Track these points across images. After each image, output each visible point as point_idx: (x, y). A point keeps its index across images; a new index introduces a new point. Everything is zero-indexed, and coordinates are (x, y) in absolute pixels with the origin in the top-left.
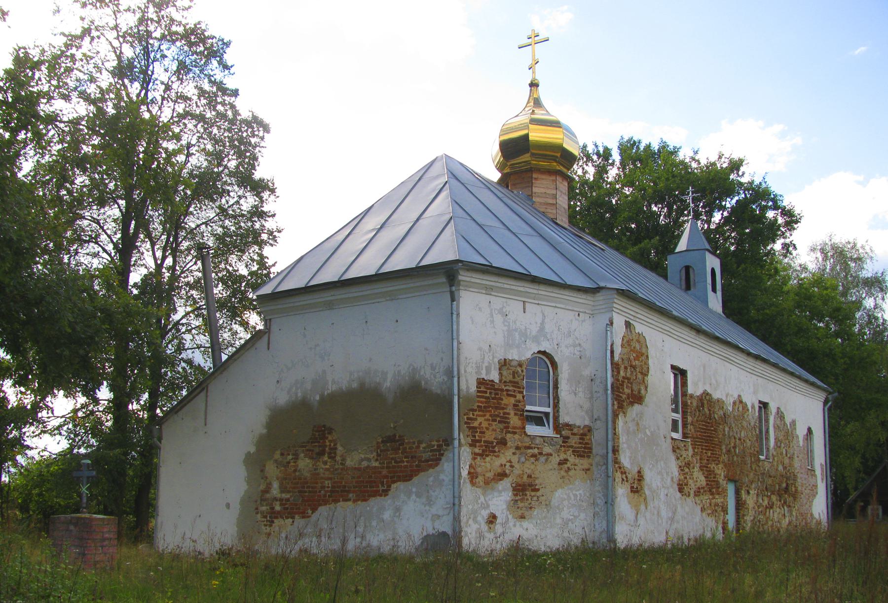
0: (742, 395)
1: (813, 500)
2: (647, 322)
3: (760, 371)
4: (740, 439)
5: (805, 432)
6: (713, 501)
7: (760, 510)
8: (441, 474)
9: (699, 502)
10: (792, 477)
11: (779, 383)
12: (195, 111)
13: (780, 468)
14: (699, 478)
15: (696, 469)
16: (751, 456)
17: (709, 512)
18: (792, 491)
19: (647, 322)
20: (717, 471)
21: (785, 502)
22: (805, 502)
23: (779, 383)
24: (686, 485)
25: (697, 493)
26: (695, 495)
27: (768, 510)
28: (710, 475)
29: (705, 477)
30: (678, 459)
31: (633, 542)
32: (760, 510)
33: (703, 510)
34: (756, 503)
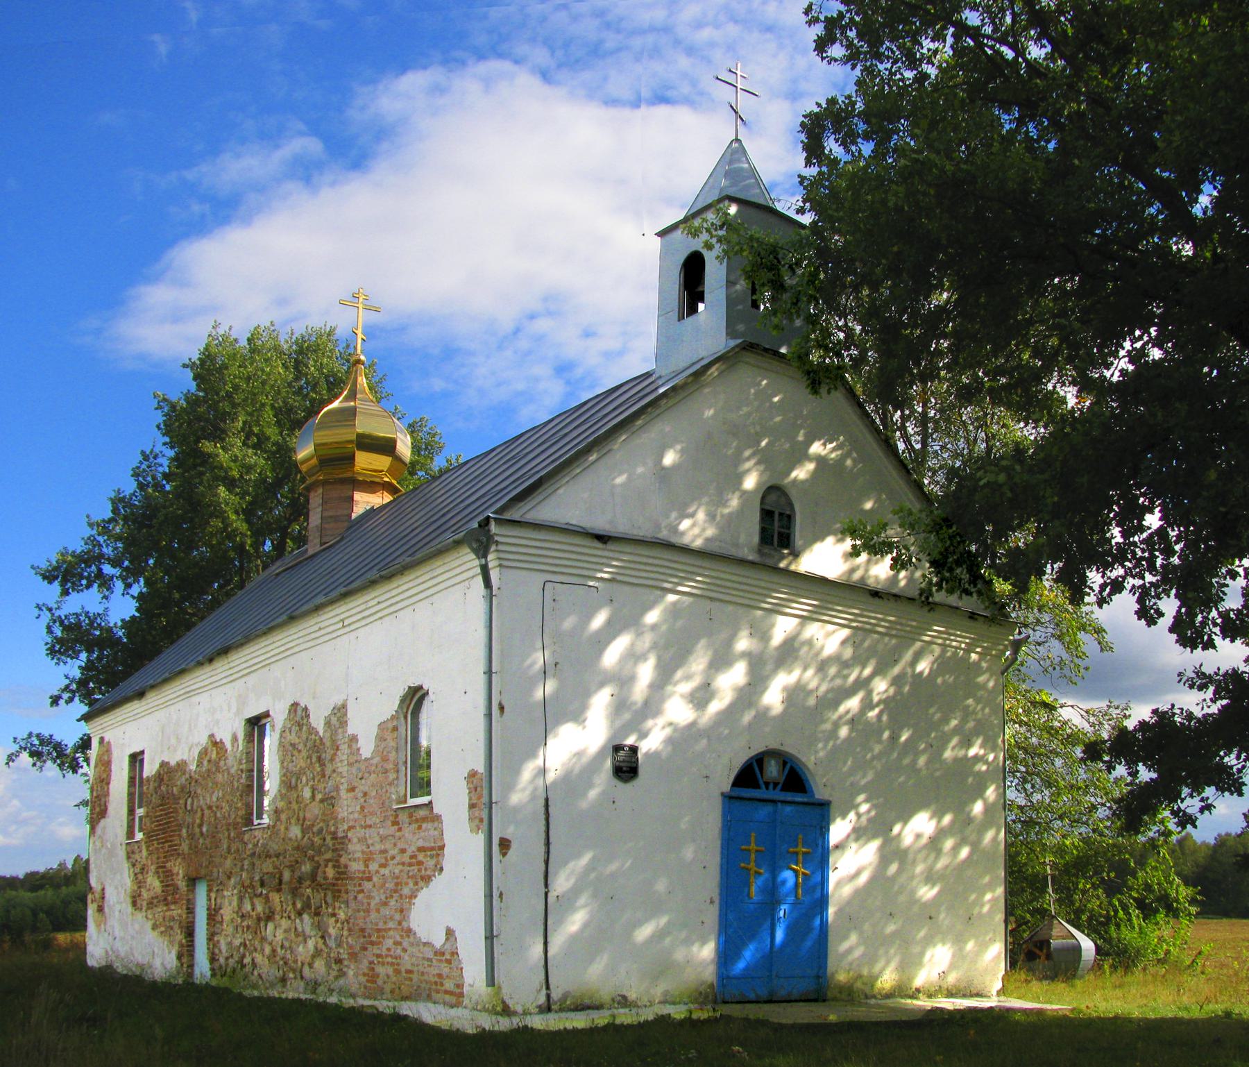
0: (215, 731)
1: (413, 896)
2: (533, 459)
3: (245, 665)
4: (210, 808)
5: (389, 706)
6: (168, 914)
7: (245, 924)
8: (1213, 788)
9: (150, 917)
10: (329, 841)
11: (296, 649)
12: (856, 125)
13: (296, 831)
14: (154, 883)
15: (150, 874)
16: (228, 830)
17: (163, 929)
18: (325, 878)
19: (533, 459)
20: (175, 870)
21: (307, 906)
22: (378, 896)
23: (296, 649)
24: (139, 896)
25: (151, 905)
26: (148, 908)
27: (262, 924)
28: (166, 875)
29: (162, 882)
30: (134, 865)
31: (169, 966)
32: (245, 924)
33: (154, 927)
34: (237, 913)
